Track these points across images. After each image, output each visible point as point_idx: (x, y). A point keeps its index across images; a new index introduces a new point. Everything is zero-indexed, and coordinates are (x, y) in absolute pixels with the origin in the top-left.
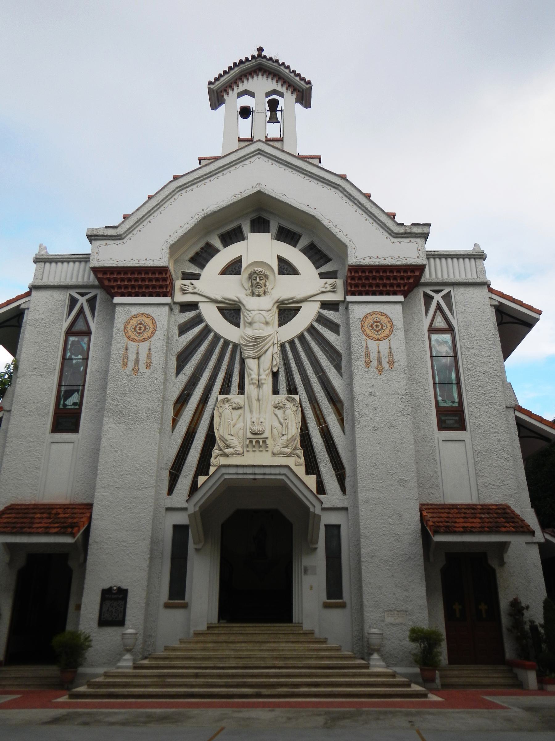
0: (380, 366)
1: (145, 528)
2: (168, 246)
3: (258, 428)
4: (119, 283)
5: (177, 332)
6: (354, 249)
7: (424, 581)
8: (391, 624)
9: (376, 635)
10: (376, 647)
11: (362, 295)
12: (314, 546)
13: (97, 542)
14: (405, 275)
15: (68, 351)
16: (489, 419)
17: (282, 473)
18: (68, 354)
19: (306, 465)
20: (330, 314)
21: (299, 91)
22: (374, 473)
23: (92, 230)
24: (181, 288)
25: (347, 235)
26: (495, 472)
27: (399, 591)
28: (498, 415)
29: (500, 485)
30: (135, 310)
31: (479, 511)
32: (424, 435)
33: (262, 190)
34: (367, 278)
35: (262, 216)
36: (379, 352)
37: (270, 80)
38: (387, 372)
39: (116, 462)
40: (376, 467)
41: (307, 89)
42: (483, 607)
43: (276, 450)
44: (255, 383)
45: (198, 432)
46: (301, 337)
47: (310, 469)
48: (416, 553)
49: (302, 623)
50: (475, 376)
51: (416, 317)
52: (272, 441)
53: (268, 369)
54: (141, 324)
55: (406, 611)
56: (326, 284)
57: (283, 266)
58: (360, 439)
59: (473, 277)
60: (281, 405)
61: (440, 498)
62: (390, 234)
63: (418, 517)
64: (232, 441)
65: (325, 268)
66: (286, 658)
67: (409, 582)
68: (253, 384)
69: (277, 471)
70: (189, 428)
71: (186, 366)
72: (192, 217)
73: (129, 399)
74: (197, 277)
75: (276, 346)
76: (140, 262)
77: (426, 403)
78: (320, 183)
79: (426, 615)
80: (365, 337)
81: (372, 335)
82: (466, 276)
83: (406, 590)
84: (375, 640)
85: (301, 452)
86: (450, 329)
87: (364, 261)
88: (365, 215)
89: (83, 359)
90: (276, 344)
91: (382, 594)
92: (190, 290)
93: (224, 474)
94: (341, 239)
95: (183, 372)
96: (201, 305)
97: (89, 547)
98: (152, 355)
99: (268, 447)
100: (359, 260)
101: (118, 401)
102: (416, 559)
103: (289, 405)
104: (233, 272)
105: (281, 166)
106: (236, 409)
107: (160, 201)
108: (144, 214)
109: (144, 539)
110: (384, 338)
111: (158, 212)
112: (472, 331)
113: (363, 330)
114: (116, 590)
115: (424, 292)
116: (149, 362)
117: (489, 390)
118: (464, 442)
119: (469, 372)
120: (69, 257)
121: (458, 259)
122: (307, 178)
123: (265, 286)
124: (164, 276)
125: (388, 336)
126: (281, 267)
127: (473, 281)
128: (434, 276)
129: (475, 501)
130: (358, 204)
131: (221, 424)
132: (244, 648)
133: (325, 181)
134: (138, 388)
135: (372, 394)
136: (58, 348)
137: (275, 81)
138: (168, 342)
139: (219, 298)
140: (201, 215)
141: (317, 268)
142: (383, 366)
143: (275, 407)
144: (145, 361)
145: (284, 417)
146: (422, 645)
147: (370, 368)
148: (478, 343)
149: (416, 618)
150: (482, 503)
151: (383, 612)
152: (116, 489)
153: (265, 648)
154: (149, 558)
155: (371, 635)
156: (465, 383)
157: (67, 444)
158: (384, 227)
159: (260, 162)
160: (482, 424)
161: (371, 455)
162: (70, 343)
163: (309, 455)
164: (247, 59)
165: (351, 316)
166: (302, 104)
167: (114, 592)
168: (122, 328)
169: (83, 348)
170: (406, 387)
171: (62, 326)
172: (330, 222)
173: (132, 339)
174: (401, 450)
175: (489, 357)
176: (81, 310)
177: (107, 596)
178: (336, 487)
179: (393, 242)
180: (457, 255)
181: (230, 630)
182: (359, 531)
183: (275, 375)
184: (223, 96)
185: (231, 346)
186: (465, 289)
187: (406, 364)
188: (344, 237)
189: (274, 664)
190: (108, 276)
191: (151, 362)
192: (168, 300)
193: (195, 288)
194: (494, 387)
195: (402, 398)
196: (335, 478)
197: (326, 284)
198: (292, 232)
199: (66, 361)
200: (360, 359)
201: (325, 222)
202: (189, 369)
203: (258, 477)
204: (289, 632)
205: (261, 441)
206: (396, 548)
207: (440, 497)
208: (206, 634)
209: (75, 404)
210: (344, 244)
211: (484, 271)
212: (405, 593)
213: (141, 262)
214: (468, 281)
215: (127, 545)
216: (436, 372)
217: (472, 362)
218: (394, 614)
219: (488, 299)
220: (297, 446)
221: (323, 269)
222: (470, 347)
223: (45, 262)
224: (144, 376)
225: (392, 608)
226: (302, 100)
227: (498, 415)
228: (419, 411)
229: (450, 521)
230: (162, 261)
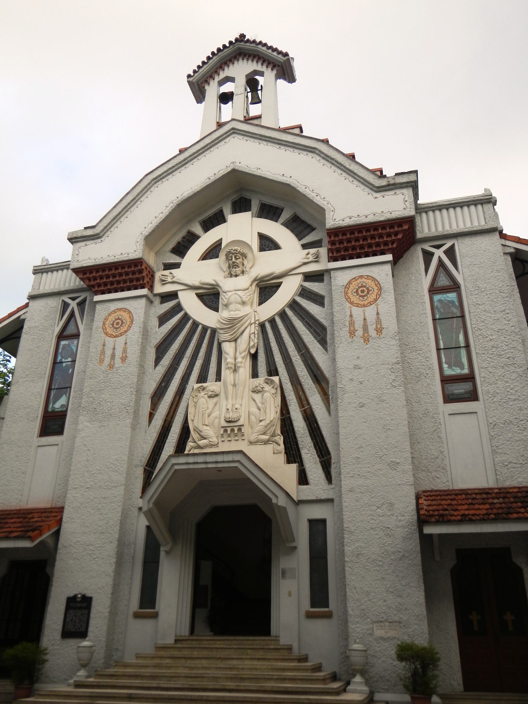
0: (366, 335)
1: (113, 530)
2: (143, 238)
3: (232, 415)
4: (98, 281)
5: (157, 323)
6: (333, 211)
7: (423, 585)
8: (382, 638)
9: (356, 652)
10: (358, 667)
11: (346, 260)
12: (294, 544)
13: (65, 547)
14: (392, 230)
16: (507, 385)
17: (236, 459)
18: (59, 358)
19: (286, 453)
20: (314, 287)
21: (279, 66)
22: (360, 456)
23: (73, 233)
24: (161, 279)
25: (324, 198)
26: (516, 448)
27: (391, 597)
28: (518, 379)
29: (524, 463)
30: (113, 306)
31: (494, 495)
32: (426, 409)
33: (236, 168)
34: (349, 241)
35: (243, 196)
36: (365, 319)
37: (250, 62)
38: (375, 341)
39: (88, 461)
40: (362, 449)
41: (285, 61)
42: (509, 617)
43: (253, 438)
44: (231, 368)
45: (173, 425)
46: (282, 314)
47: (291, 458)
48: (411, 549)
49: (279, 637)
50: (487, 336)
51: (413, 278)
52: (250, 429)
53: (245, 351)
54: (119, 319)
55: (400, 622)
56: (308, 254)
57: (265, 243)
58: (343, 418)
59: (482, 224)
60: (259, 388)
61: (447, 483)
62: (372, 189)
63: (413, 506)
64: (208, 431)
65: (309, 239)
66: (242, 679)
67: (404, 586)
69: (229, 458)
70: (165, 421)
71: (164, 358)
72: (166, 207)
73: (103, 396)
74: (177, 266)
75: (253, 326)
76: (116, 257)
77: (428, 372)
78: (296, 150)
79: (425, 627)
80: (349, 305)
81: (358, 302)
82: (472, 224)
83: (400, 596)
84: (357, 659)
85: (280, 439)
86: (455, 287)
87: (343, 222)
88: (344, 174)
89: (72, 361)
90: (254, 324)
91: (370, 601)
92: (169, 280)
93: (174, 465)
94: (318, 203)
95: (161, 363)
97: (58, 552)
98: (128, 349)
99: (243, 435)
100: (338, 222)
101: (93, 398)
102: (411, 557)
103: (267, 388)
104: (213, 256)
105: (256, 141)
106: (213, 397)
107: (135, 195)
108: (120, 210)
109: (111, 542)
110: (370, 304)
111: (135, 206)
112: (481, 285)
113: (347, 297)
114: (80, 598)
115: (422, 249)
116: (124, 356)
117: (505, 350)
118: (476, 414)
119: (480, 332)
120: (62, 264)
121: (461, 207)
122: (282, 147)
123: (243, 265)
124: (139, 268)
125: (376, 300)
126: (262, 245)
127: (480, 228)
128: (433, 229)
129: (491, 483)
130: (336, 164)
132: (200, 666)
133: (300, 147)
134: (113, 383)
136: (49, 353)
137: (255, 62)
138: (145, 333)
139: (197, 283)
140: (176, 202)
141: (300, 239)
142: (369, 333)
143: (253, 392)
144: (121, 356)
145: (262, 402)
146: (413, 666)
147: (355, 337)
148: (489, 298)
149: (413, 631)
150: (500, 486)
151: (371, 623)
153: (222, 666)
154: (115, 562)
155: (353, 652)
156: (475, 345)
157: (52, 447)
158: (365, 183)
159: (235, 141)
160: (499, 391)
161: (356, 436)
162: (61, 347)
163: (290, 442)
164: (224, 46)
165: (333, 283)
166: (285, 79)
167: (79, 600)
168: (101, 324)
169: (72, 350)
170: (396, 355)
171: (54, 332)
172: (306, 188)
173: (109, 335)
174: (392, 428)
175: (503, 312)
176: (72, 314)
177: (72, 604)
178: (320, 475)
179: (376, 198)
180: (459, 203)
181: (199, 644)
182: (343, 526)
183: (254, 357)
184: (204, 87)
185: (209, 332)
186: (471, 239)
187: (396, 329)
188: (321, 200)
189: (224, 685)
190: (88, 275)
191: (126, 357)
192: (144, 291)
193: (174, 277)
194: (511, 346)
195: (393, 368)
196: (319, 466)
197: (308, 254)
198: (274, 207)
199: (57, 365)
200: (344, 330)
201: (301, 189)
203: (210, 466)
204: (258, 647)
205: (236, 429)
206: (386, 544)
207: (448, 481)
208: (173, 648)
209: (62, 406)
210: (322, 208)
211: (496, 215)
212: (399, 599)
213: (117, 257)
214: (474, 229)
215: (94, 549)
216: (440, 336)
217: (482, 320)
218: (385, 626)
219: (500, 248)
220: (276, 432)
221: (305, 241)
222: (480, 303)
223: (42, 273)
224: (119, 371)
225: (382, 618)
226: (284, 75)
227: (518, 379)
228: (420, 383)
229: (449, 509)
230: (137, 253)
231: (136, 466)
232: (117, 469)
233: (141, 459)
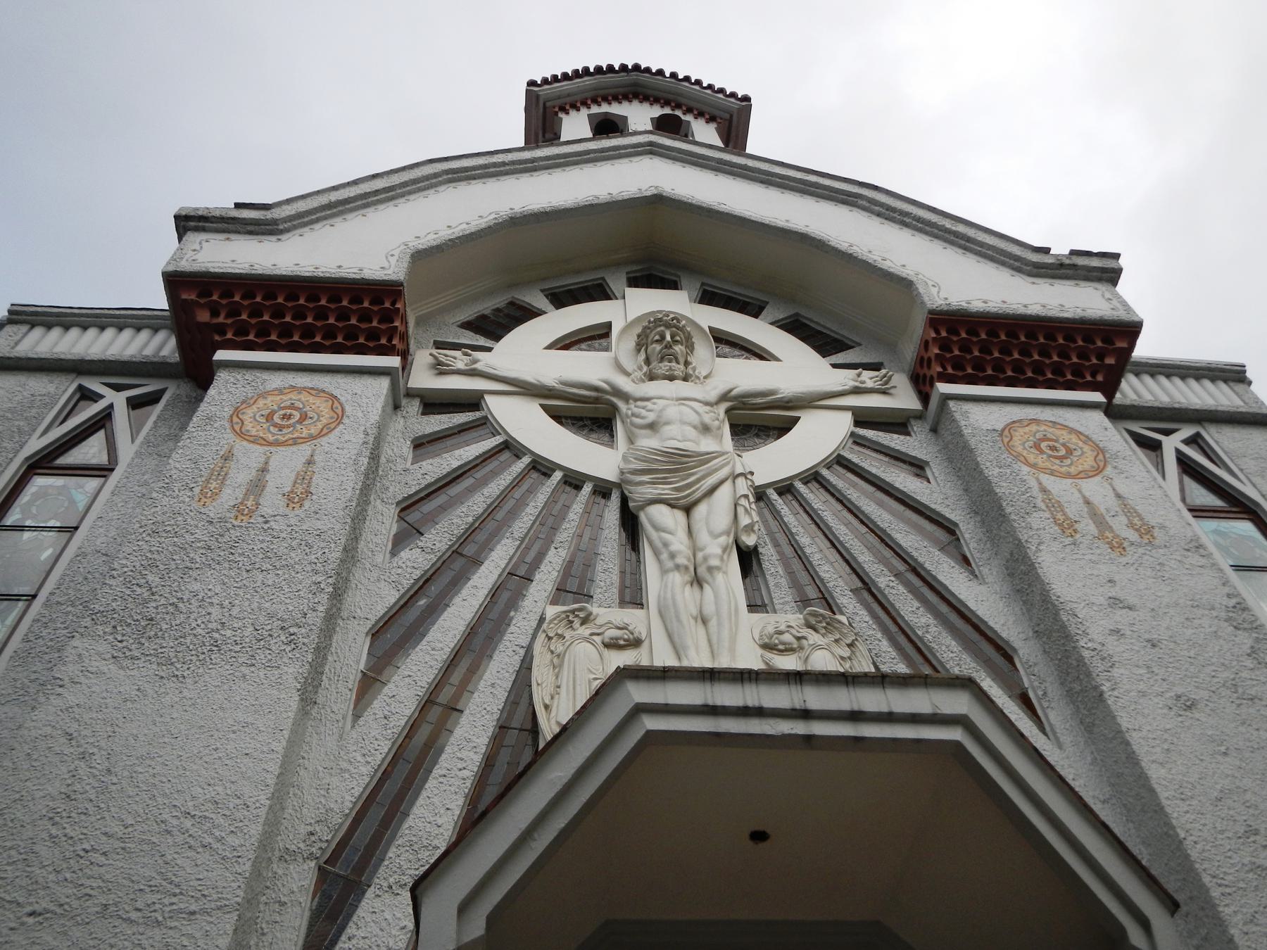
15: (18, 510)
30: (276, 380)
44: (687, 568)
60: (787, 637)
68: (677, 567)
93: (640, 709)
96: (489, 399)
131: (563, 690)
135: (1115, 602)
152: (31, 920)
173: (251, 439)
202: (439, 538)
231: (288, 856)
232: (208, 840)
233: (310, 829)
